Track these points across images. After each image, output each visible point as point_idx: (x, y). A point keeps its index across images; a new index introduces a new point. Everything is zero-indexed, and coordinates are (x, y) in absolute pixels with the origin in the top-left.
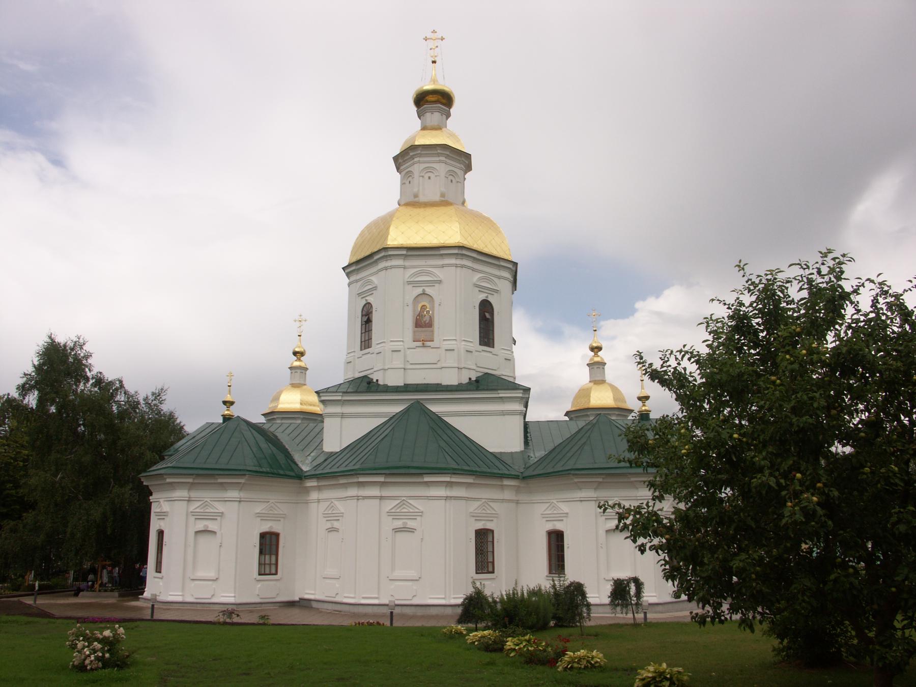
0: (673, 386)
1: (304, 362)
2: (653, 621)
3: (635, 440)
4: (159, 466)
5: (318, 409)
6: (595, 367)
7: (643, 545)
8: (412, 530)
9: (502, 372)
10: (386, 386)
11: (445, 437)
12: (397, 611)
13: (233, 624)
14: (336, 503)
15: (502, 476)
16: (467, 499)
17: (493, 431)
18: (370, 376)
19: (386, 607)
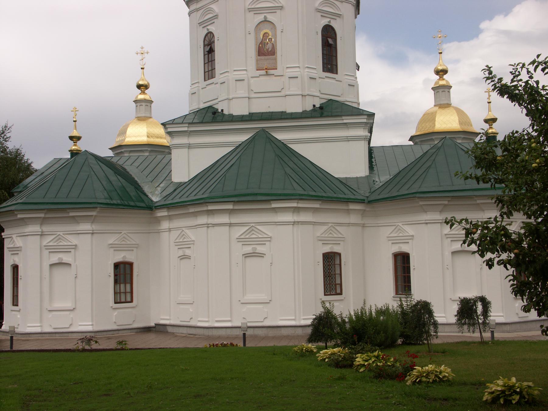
0: (523, 101)
1: (149, 94)
2: (501, 340)
3: (483, 156)
4: (9, 203)
5: (165, 141)
6: (440, 90)
7: (490, 260)
8: (261, 255)
9: (346, 98)
10: (292, 113)
11: (291, 164)
12: (249, 332)
13: (92, 351)
14: (187, 231)
15: (347, 201)
16: (314, 223)
17: (338, 156)
18: (215, 106)
19: (238, 329)
